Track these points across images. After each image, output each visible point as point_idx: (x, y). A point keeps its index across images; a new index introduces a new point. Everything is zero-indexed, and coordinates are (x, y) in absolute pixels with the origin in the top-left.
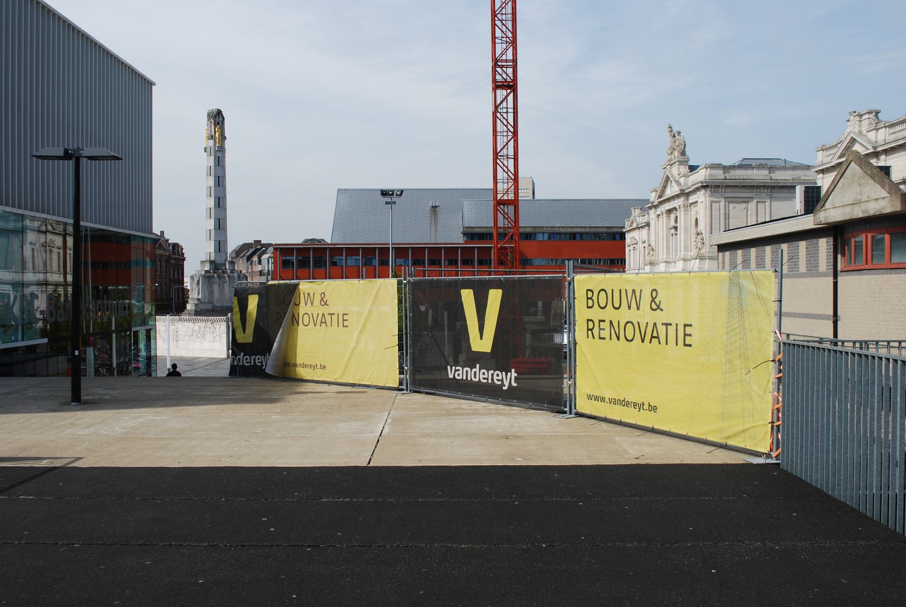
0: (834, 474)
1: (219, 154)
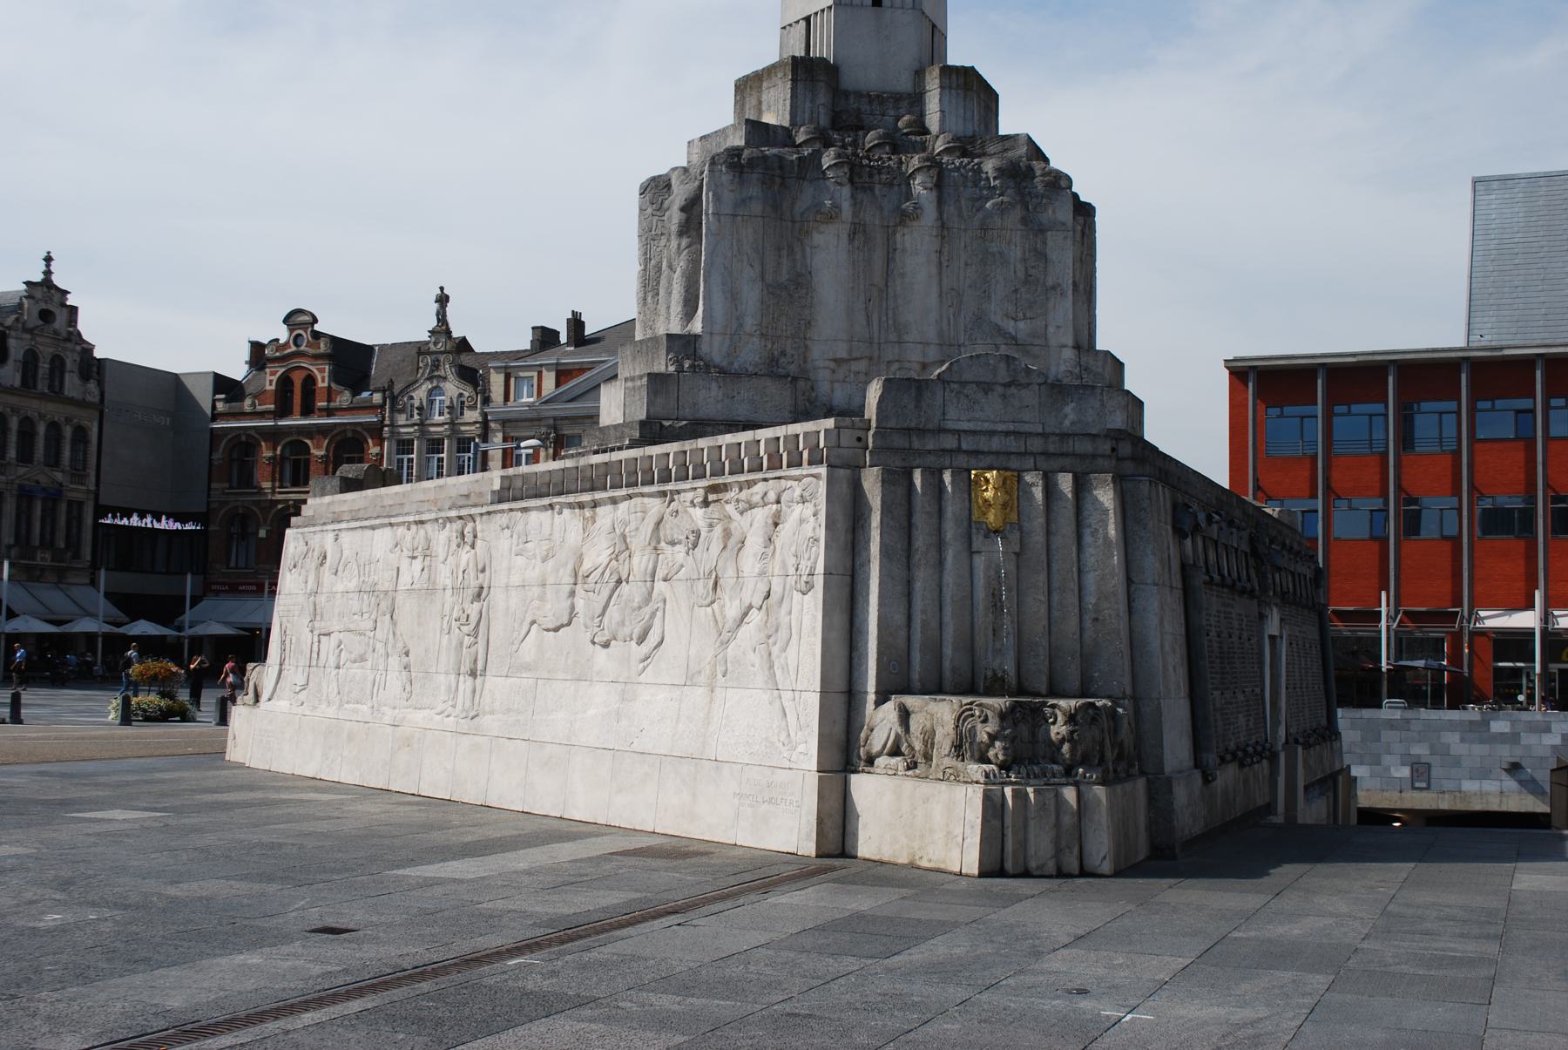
0: (996, 605)
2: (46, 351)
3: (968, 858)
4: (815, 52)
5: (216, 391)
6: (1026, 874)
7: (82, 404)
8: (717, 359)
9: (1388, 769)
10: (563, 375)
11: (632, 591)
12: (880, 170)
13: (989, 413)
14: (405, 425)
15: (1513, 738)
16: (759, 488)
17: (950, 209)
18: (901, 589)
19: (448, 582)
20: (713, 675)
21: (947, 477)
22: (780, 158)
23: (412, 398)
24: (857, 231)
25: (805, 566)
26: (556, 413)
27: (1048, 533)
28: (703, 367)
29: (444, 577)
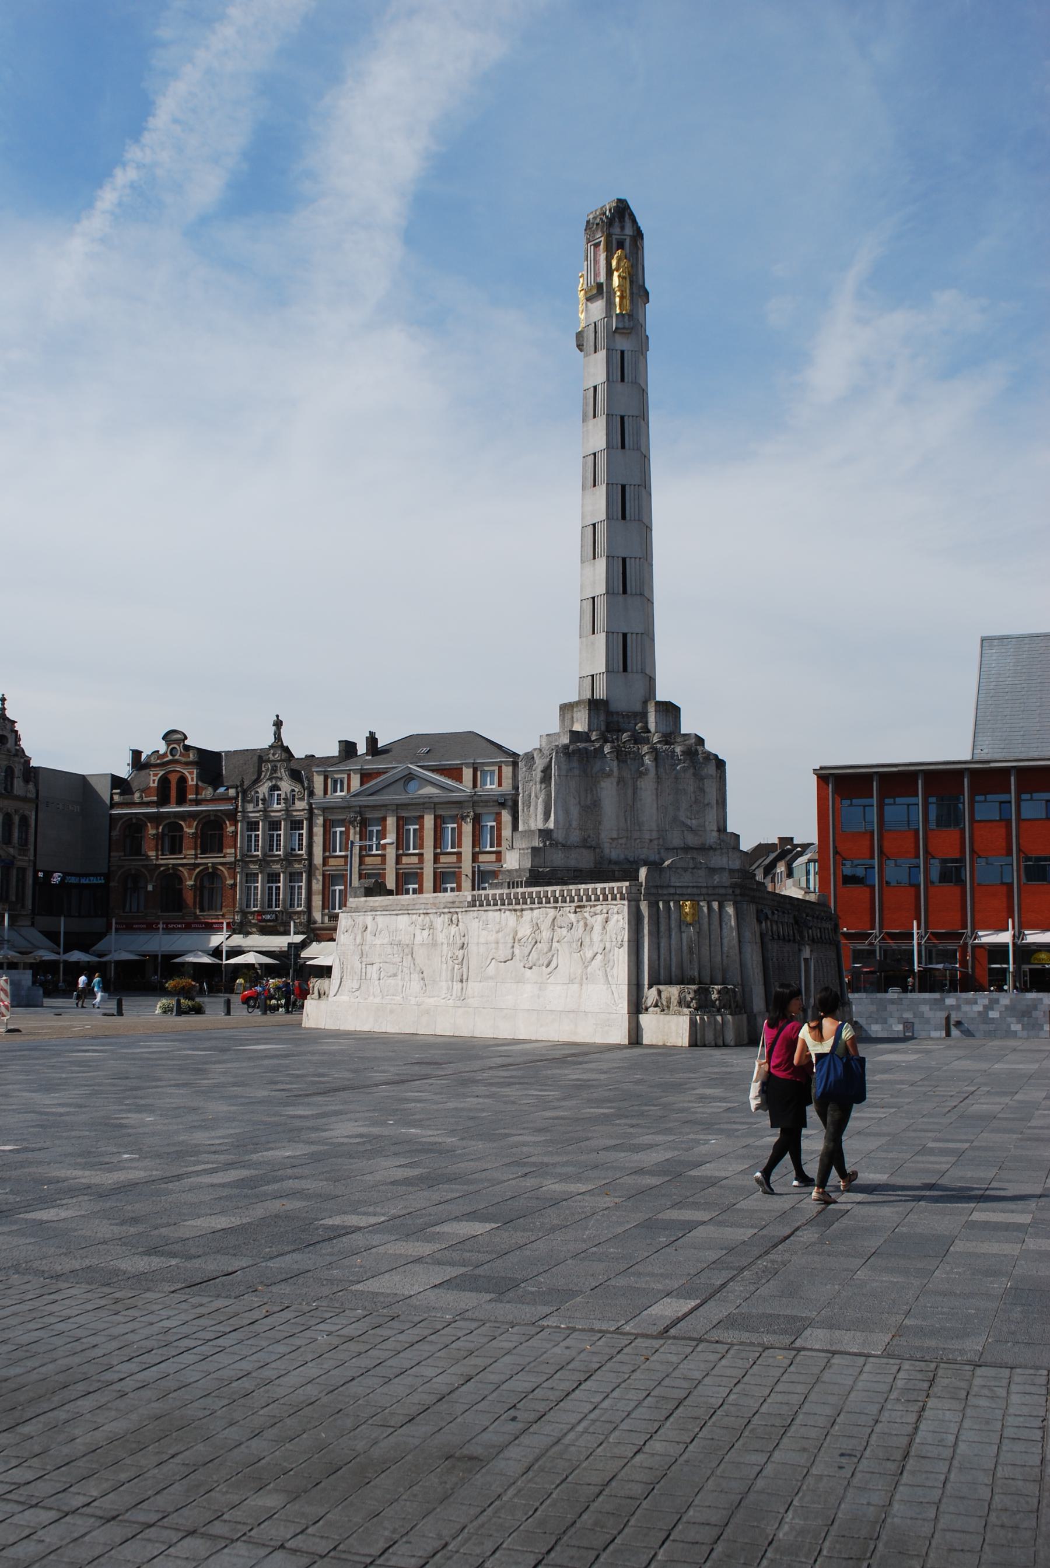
0: (691, 952)
1: (622, 343)
3: (685, 1041)
4: (597, 696)
5: (113, 787)
6: (705, 1046)
7: (24, 799)
8: (560, 840)
9: (891, 1026)
11: (543, 946)
12: (629, 753)
13: (687, 879)
14: (253, 811)
15: (958, 1007)
16: (599, 908)
17: (661, 770)
18: (656, 946)
19: (445, 941)
20: (582, 979)
21: (672, 904)
22: (586, 749)
23: (257, 792)
24: (621, 781)
25: (620, 939)
26: (361, 803)
27: (709, 924)
29: (441, 938)
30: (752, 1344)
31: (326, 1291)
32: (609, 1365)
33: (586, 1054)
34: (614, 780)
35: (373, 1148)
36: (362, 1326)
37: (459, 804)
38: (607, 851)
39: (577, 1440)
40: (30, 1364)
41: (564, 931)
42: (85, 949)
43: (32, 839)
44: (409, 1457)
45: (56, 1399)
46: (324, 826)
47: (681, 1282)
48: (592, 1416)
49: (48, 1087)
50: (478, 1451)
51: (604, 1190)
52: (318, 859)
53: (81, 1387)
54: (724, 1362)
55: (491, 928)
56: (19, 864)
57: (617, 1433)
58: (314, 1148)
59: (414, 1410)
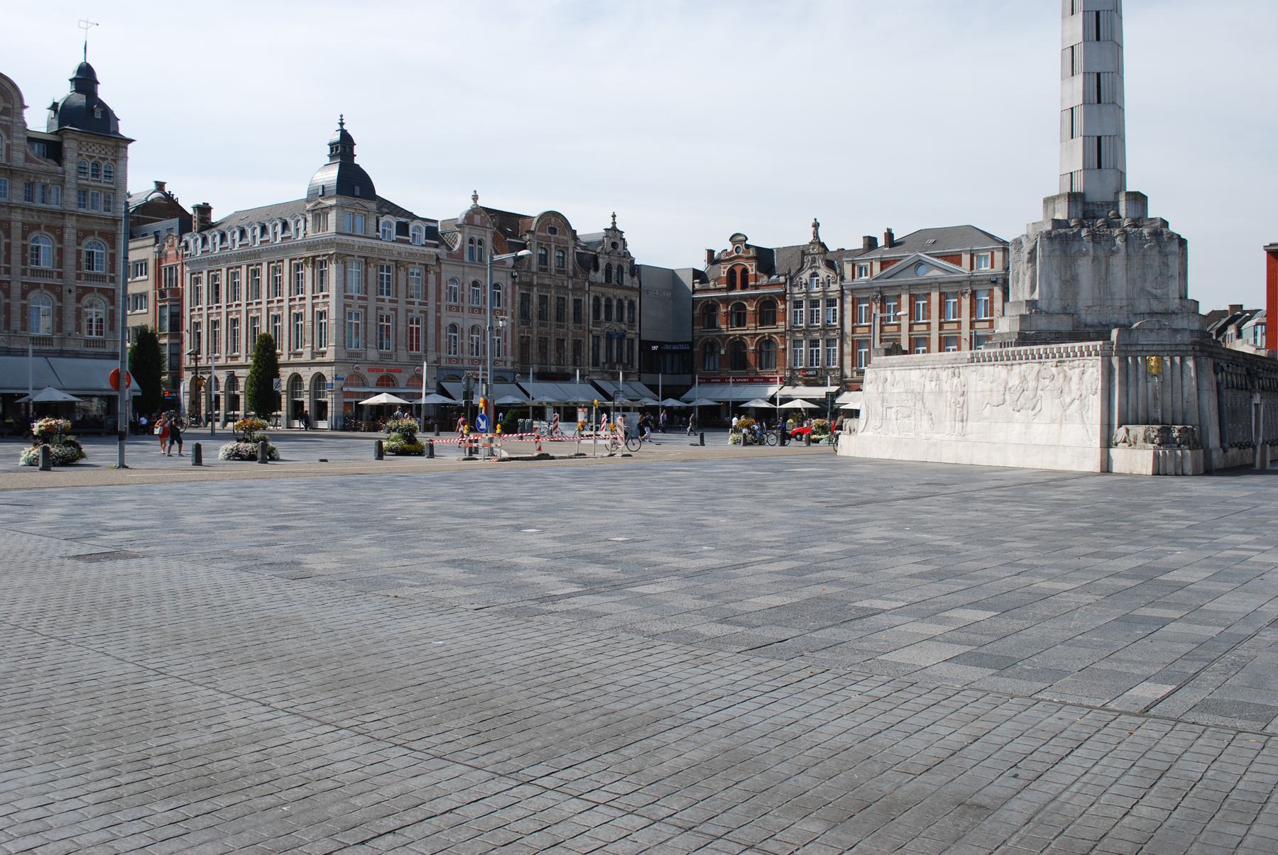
0: (1155, 398)
2: (615, 263)
3: (1149, 470)
7: (631, 289)
10: (884, 264)
13: (1153, 338)
14: (798, 293)
17: (1130, 249)
24: (1095, 259)
28: (1039, 312)
29: (946, 387)
30: (1225, 727)
31: (858, 659)
32: (1097, 736)
33: (1065, 479)
34: (1089, 259)
35: (894, 548)
36: (887, 689)
37: (959, 283)
38: (1083, 317)
39: (1070, 799)
40: (632, 701)
41: (1047, 382)
42: (677, 398)
43: (637, 317)
44: (927, 801)
45: (650, 730)
46: (853, 302)
47: (1158, 669)
48: (1084, 779)
49: (650, 496)
50: (986, 801)
51: (1086, 589)
52: (848, 329)
53: (669, 722)
54: (1200, 741)
55: (986, 380)
56: (629, 336)
57: (1106, 796)
58: (848, 547)
59: (930, 762)
